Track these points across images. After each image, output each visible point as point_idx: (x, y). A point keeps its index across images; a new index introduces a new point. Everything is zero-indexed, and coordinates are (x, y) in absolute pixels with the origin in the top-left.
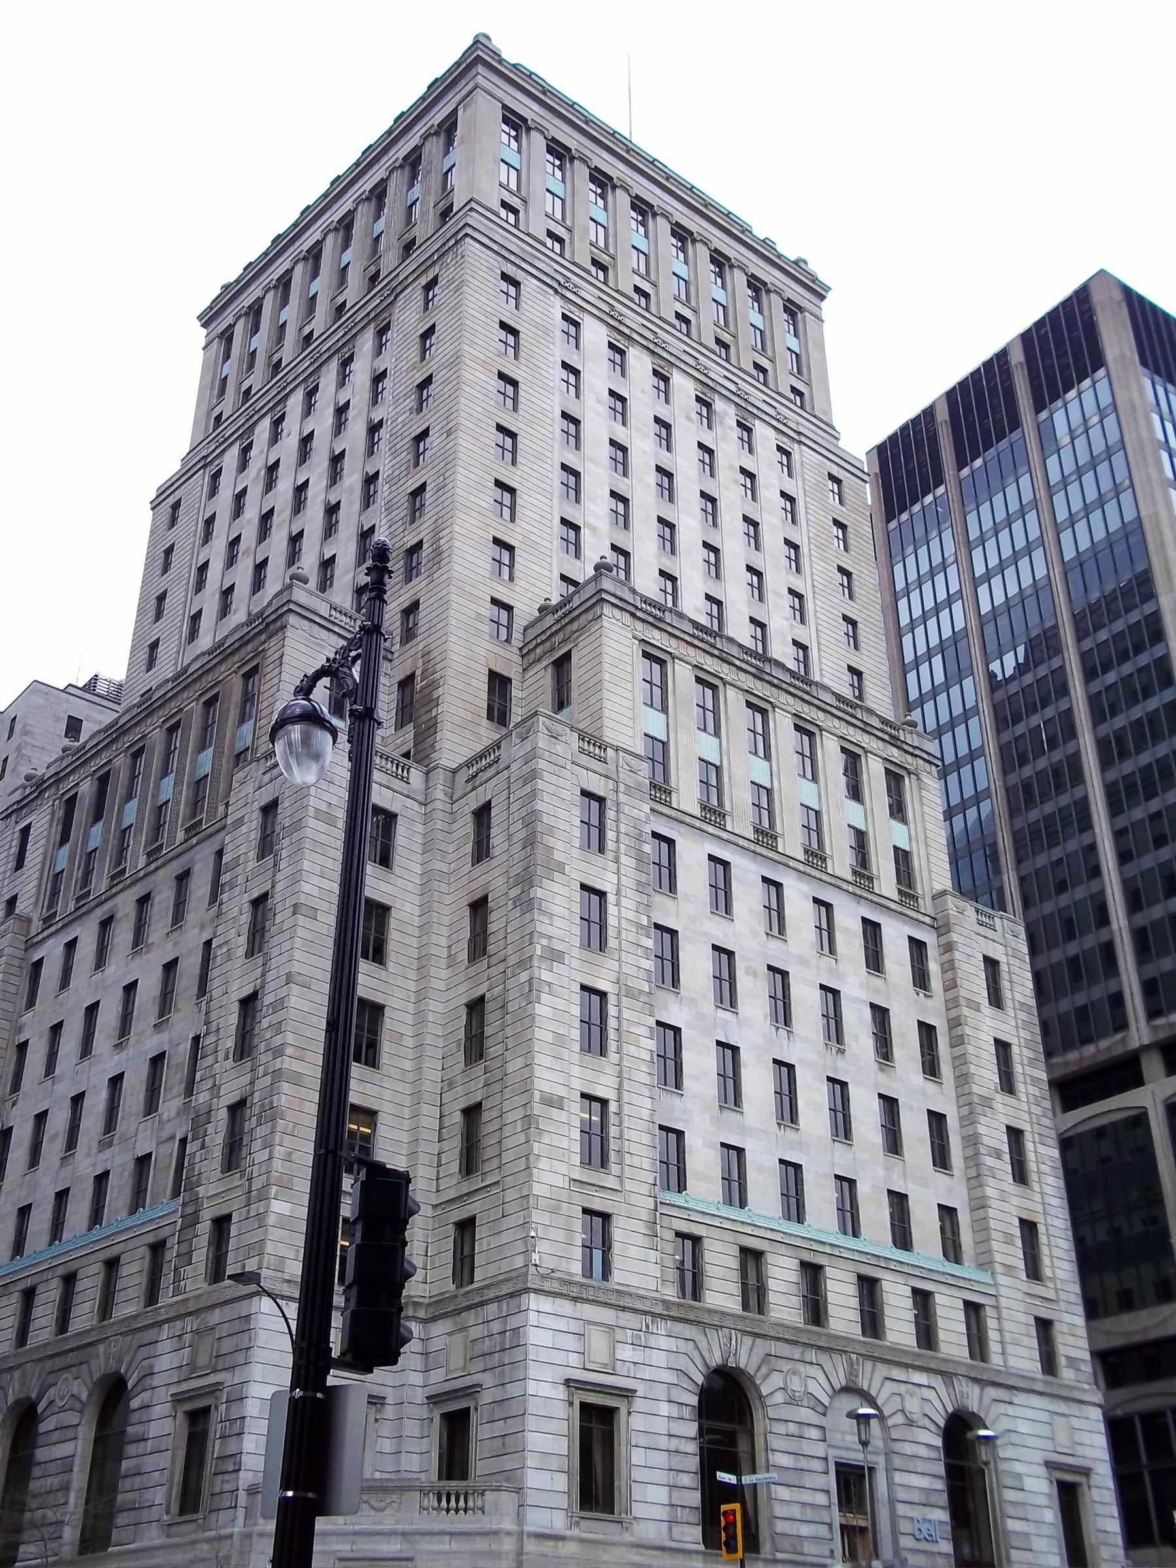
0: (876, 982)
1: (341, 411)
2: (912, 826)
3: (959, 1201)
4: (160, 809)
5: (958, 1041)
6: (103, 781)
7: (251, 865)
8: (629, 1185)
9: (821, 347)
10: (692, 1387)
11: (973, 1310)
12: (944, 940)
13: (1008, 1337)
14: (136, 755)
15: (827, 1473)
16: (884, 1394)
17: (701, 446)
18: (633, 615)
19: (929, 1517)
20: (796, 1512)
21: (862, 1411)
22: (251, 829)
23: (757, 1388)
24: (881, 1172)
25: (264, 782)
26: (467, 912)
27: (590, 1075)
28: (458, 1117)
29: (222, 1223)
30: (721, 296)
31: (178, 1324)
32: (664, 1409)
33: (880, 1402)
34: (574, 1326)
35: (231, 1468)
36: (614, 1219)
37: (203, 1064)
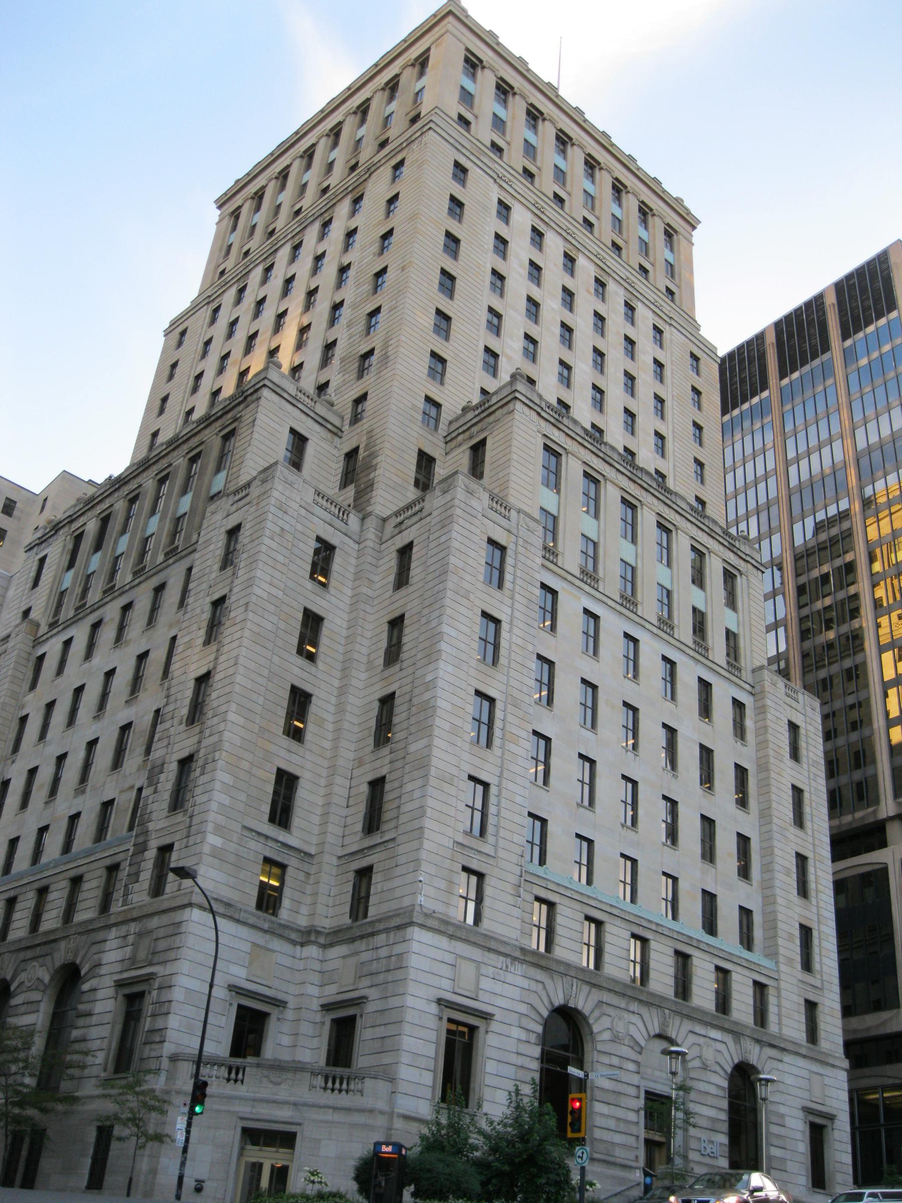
0: (703, 726)
2: (740, 614)
3: (754, 905)
5: (765, 784)
6: (105, 521)
7: (213, 575)
8: (501, 854)
10: (538, 1018)
11: (760, 988)
12: (760, 704)
14: (132, 501)
15: (638, 1097)
18: (539, 414)
19: (713, 1139)
20: (612, 1124)
25: (231, 512)
26: (386, 627)
27: (478, 762)
28: (365, 788)
31: (123, 930)
32: (516, 1033)
34: (449, 958)
35: (158, 1039)
37: (159, 728)
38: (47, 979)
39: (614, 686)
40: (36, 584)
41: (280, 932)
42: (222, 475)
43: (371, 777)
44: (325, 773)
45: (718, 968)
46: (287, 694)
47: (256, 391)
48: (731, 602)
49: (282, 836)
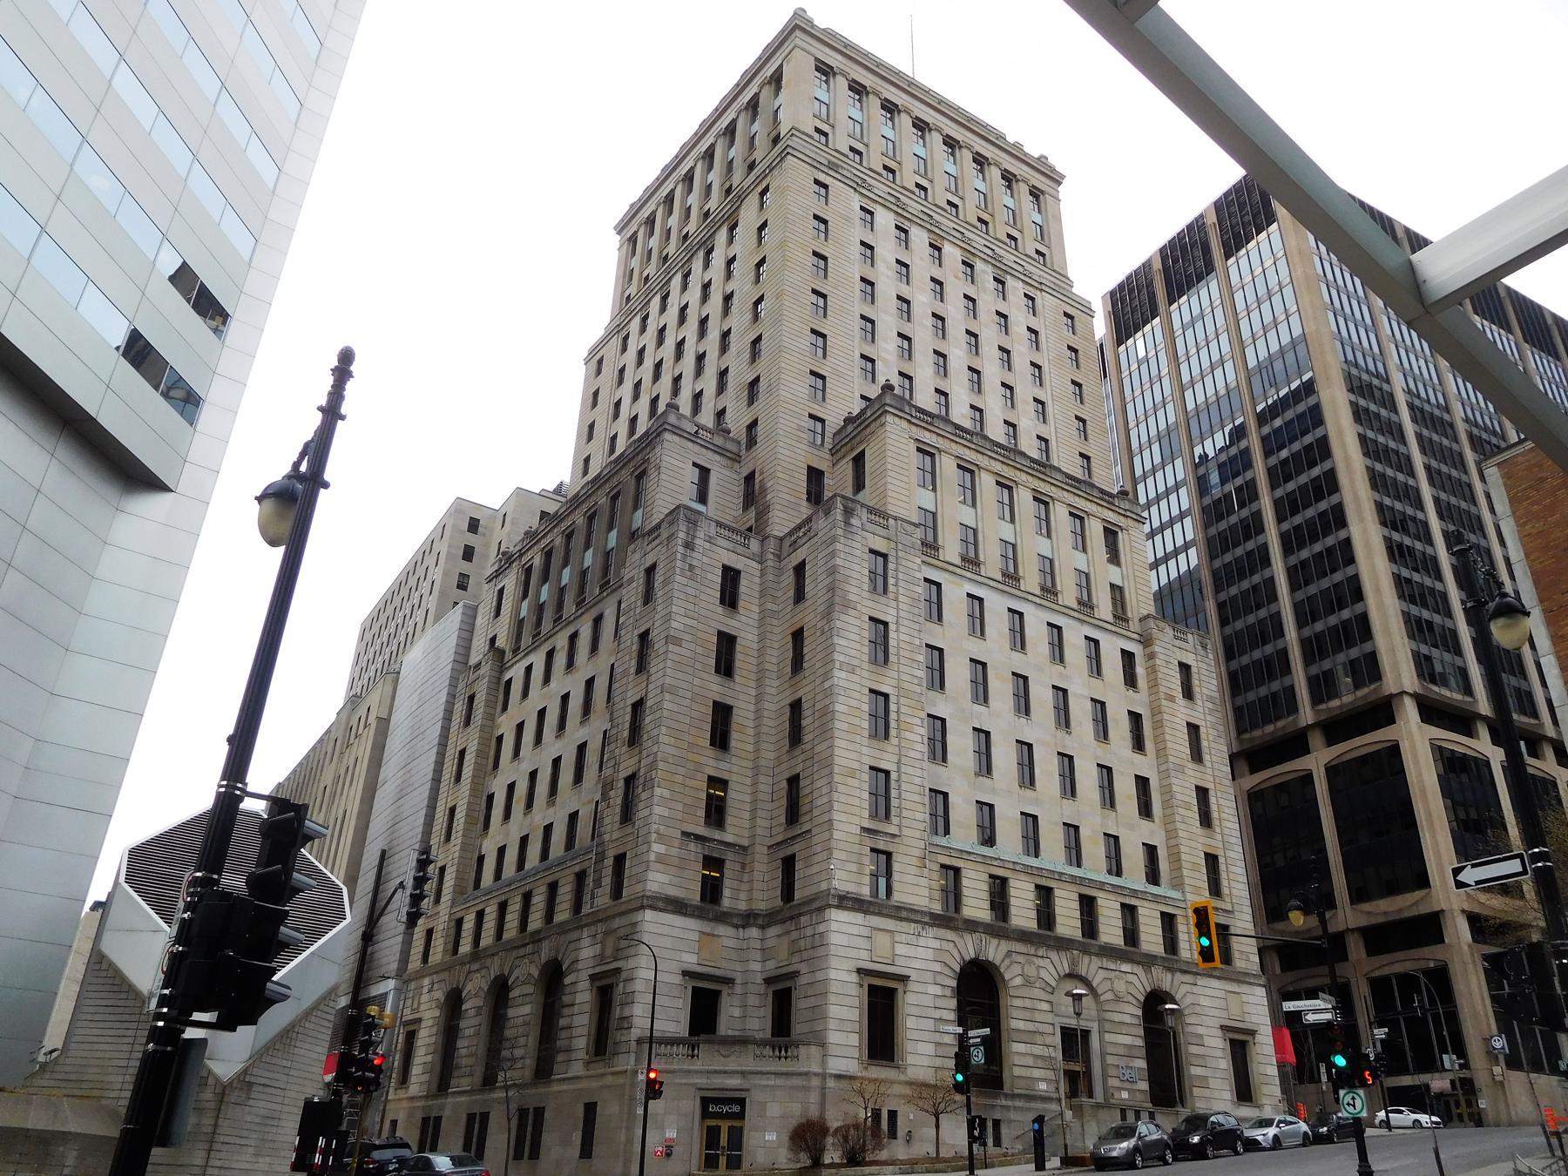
1: (706, 287)
3: (1158, 840)
4: (584, 573)
5: (1158, 725)
6: (548, 555)
8: (905, 832)
9: (1058, 219)
12: (1148, 650)
20: (1030, 1061)
22: (638, 586)
24: (1098, 819)
26: (790, 638)
27: (877, 753)
28: (784, 784)
29: (620, 860)
30: (981, 186)
31: (593, 928)
34: (865, 932)
38: (536, 973)
40: (498, 613)
41: (723, 918)
42: (640, 512)
44: (750, 773)
48: (1114, 557)
49: (717, 835)
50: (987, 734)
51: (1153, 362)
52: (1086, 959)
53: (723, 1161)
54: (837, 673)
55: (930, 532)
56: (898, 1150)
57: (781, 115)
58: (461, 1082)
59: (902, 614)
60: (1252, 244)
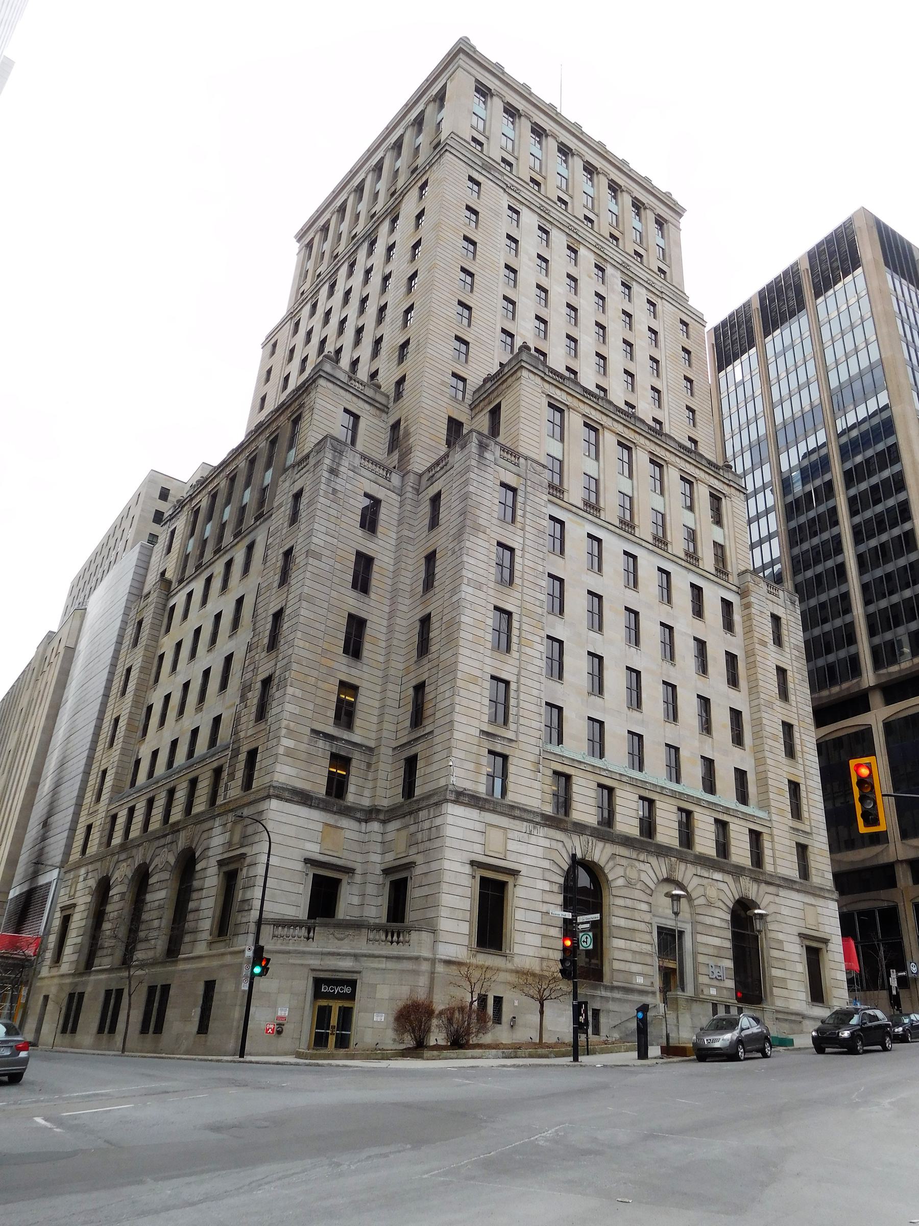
0: (697, 622)
5: (752, 666)
6: (214, 497)
7: (284, 531)
8: (522, 738)
9: (678, 245)
11: (756, 837)
12: (745, 601)
13: (777, 854)
16: (692, 884)
17: (597, 294)
18: (542, 378)
20: (629, 956)
21: (674, 892)
23: (605, 875)
26: (423, 561)
27: (498, 664)
28: (411, 691)
29: (252, 754)
31: (225, 817)
33: (689, 889)
34: (480, 827)
36: (510, 759)
38: (172, 860)
39: (617, 595)
41: (347, 812)
42: (293, 451)
43: (414, 683)
44: (380, 681)
45: (717, 821)
46: (345, 622)
47: (314, 381)
48: (718, 520)
49: (346, 735)
50: (600, 658)
51: (748, 385)
52: (682, 866)
53: (332, 1040)
54: (464, 587)
55: (556, 477)
56: (502, 1034)
57: (443, 125)
58: (104, 962)
59: (528, 542)
60: (839, 285)
